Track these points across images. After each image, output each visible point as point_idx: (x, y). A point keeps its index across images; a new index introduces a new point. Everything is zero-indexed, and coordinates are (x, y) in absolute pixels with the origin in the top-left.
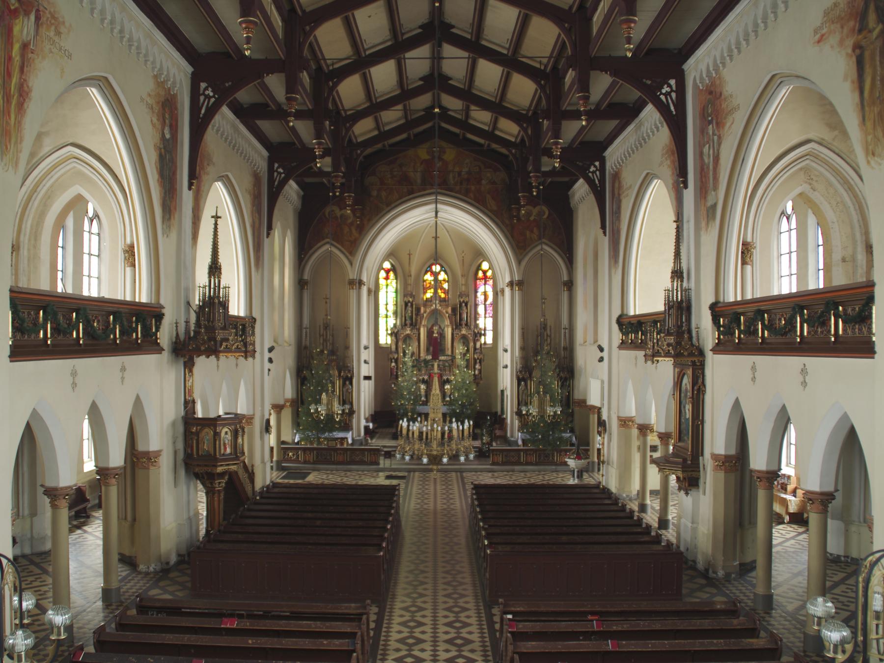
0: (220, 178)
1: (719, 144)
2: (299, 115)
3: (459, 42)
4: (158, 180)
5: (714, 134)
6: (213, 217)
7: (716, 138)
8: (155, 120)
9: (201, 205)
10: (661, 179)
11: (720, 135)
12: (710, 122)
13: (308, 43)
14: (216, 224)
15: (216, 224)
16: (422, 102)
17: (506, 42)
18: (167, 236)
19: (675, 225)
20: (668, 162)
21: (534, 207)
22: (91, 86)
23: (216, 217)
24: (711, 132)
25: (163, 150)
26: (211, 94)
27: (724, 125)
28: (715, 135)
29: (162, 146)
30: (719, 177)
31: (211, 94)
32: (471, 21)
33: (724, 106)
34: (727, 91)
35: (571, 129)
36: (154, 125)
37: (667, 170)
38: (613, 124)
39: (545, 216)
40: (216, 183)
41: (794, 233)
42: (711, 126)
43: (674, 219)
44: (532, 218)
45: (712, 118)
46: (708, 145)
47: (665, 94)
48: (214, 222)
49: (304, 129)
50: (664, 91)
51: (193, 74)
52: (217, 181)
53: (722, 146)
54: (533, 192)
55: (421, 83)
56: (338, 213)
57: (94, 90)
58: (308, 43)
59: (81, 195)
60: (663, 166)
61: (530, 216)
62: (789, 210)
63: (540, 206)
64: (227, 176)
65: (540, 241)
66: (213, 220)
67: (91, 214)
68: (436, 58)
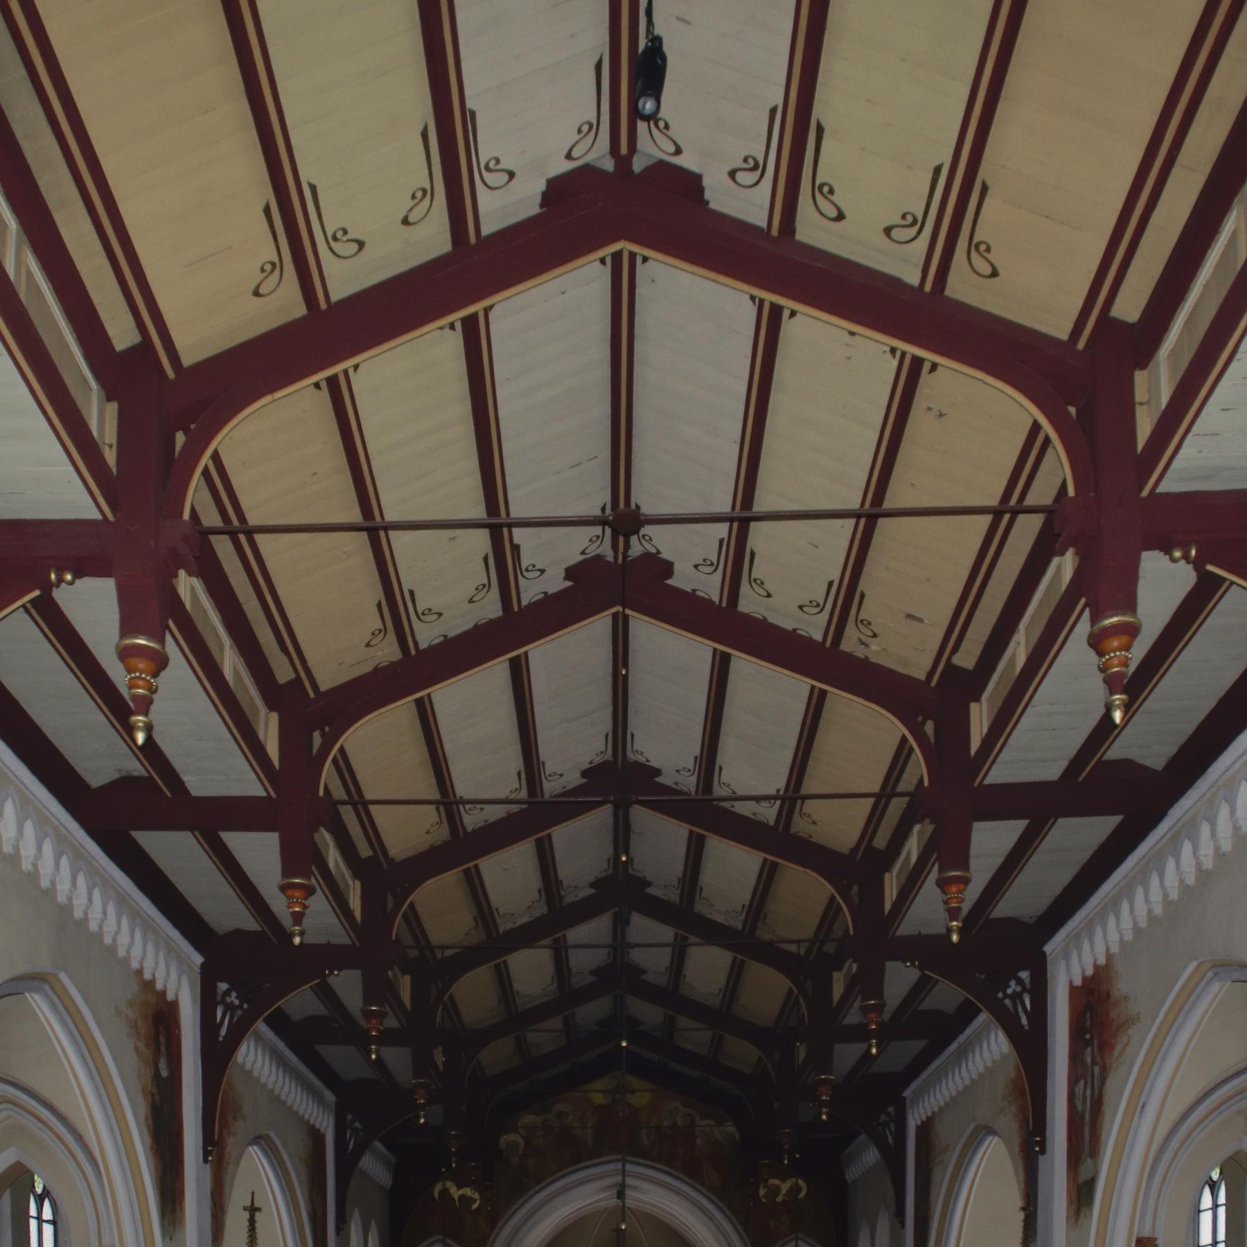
0: (256, 1140)
1: (1103, 1081)
2: (387, 1038)
3: (659, 910)
4: (152, 1148)
5: (1094, 1063)
6: (245, 1209)
7: (1097, 1069)
8: (141, 1045)
9: (227, 1189)
10: (1000, 1137)
11: (1105, 1064)
12: (1089, 1043)
13: (401, 914)
14: (252, 1222)
15: (252, 1222)
16: (592, 1012)
17: (740, 911)
18: (171, 1239)
19: (1021, 1215)
20: (1013, 1108)
21: (784, 1181)
22: (31, 990)
23: (253, 1210)
24: (1089, 1060)
25: (157, 1098)
26: (237, 1002)
27: (1112, 1048)
28: (1097, 1064)
29: (155, 1090)
30: (1101, 1134)
31: (237, 1002)
32: (681, 875)
33: (1113, 1014)
34: (1119, 990)
35: (846, 1055)
36: (140, 1055)
37: (1009, 1123)
38: (917, 1045)
39: (802, 1195)
40: (250, 1148)
41: (1222, 1212)
42: (1089, 1050)
43: (1021, 1206)
44: (779, 1199)
45: (1092, 1037)
46: (1083, 1082)
47: (1011, 997)
48: (248, 1217)
49: (398, 1060)
50: (1009, 991)
51: (203, 966)
52: (250, 1144)
53: (1108, 1083)
54: (784, 1159)
55: (593, 891)
56: (456, 1193)
57: (36, 997)
58: (401, 914)
59: (21, 1163)
60: (1005, 1115)
61: (777, 1196)
62: (1215, 1175)
63: (794, 1180)
64: (268, 1136)
65: (794, 1236)
66: (247, 1215)
67: (39, 1190)
68: (622, 835)
